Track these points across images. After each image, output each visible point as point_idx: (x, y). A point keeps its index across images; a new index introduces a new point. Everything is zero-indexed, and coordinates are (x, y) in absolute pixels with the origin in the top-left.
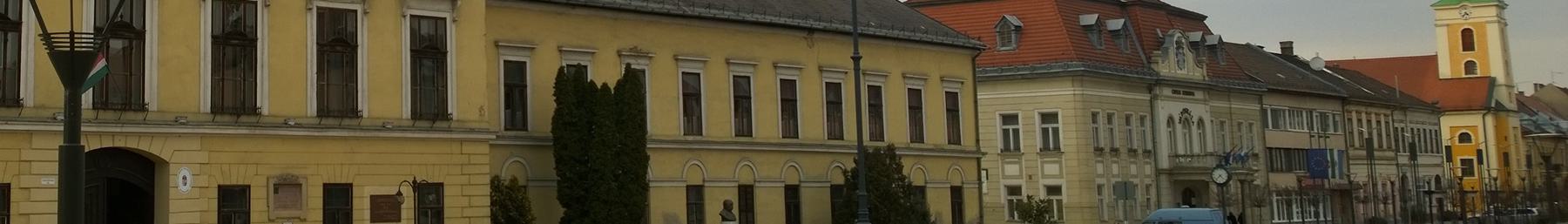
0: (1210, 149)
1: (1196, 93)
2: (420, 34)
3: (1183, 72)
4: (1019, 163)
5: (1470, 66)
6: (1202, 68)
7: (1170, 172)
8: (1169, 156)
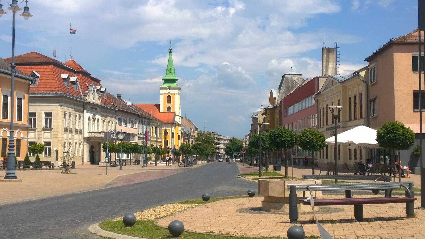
3: (94, 100)
4: (51, 133)
5: (169, 108)
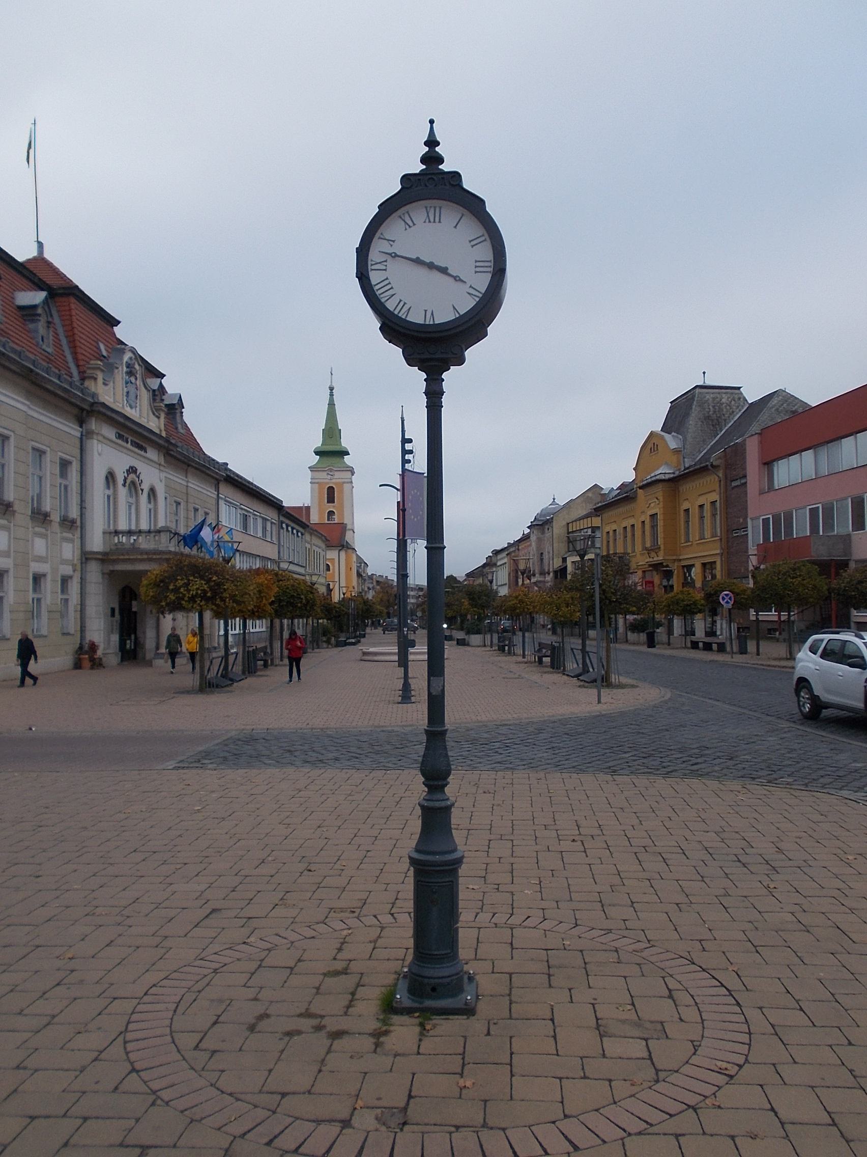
0: (161, 523)
1: (149, 449)
2: (10, 534)
6: (158, 418)
7: (104, 558)
8: (104, 533)
